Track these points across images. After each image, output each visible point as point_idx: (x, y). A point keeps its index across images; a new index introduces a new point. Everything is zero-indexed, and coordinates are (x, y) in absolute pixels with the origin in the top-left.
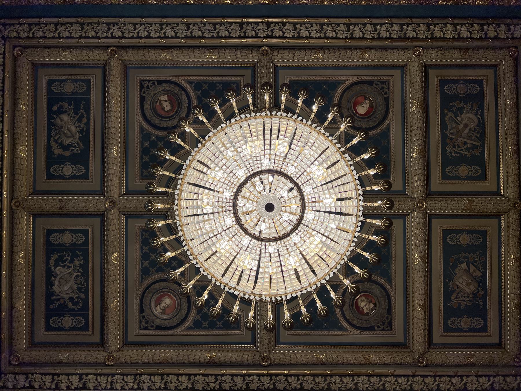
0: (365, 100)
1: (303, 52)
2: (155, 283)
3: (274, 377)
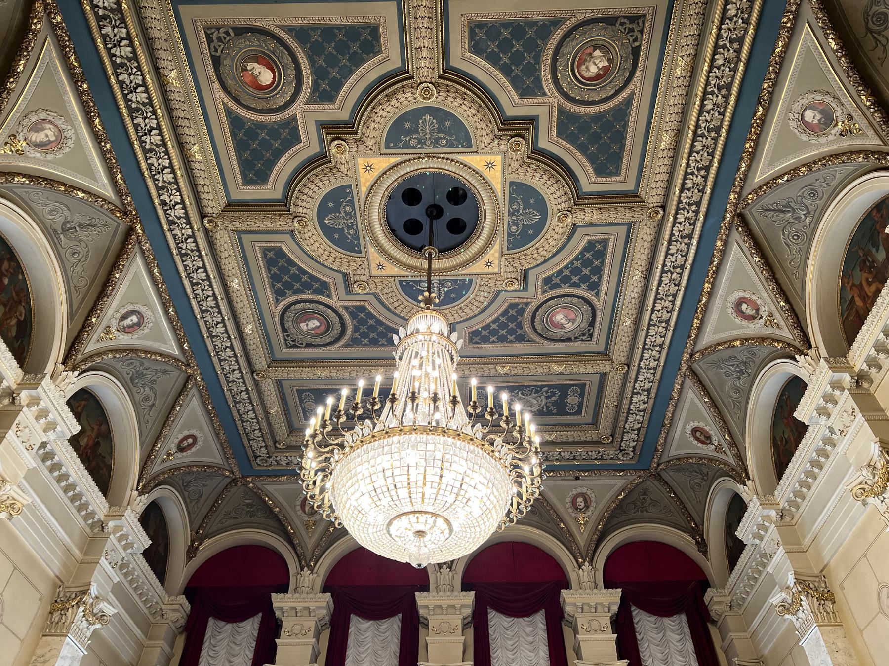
0: (247, 70)
1: (196, 173)
2: (535, 329)
3: (681, 206)
